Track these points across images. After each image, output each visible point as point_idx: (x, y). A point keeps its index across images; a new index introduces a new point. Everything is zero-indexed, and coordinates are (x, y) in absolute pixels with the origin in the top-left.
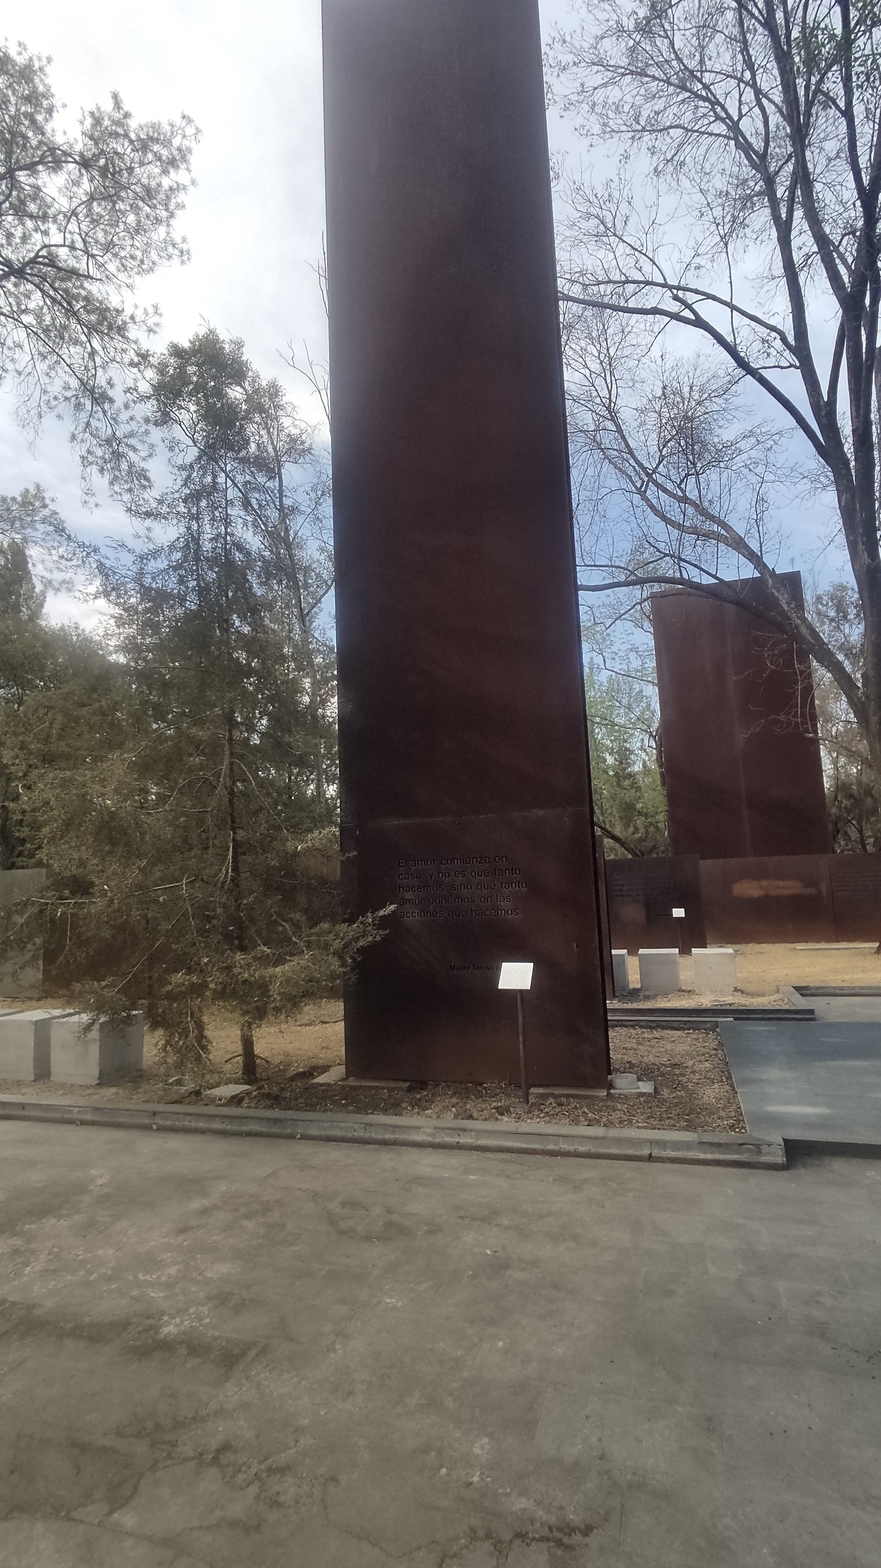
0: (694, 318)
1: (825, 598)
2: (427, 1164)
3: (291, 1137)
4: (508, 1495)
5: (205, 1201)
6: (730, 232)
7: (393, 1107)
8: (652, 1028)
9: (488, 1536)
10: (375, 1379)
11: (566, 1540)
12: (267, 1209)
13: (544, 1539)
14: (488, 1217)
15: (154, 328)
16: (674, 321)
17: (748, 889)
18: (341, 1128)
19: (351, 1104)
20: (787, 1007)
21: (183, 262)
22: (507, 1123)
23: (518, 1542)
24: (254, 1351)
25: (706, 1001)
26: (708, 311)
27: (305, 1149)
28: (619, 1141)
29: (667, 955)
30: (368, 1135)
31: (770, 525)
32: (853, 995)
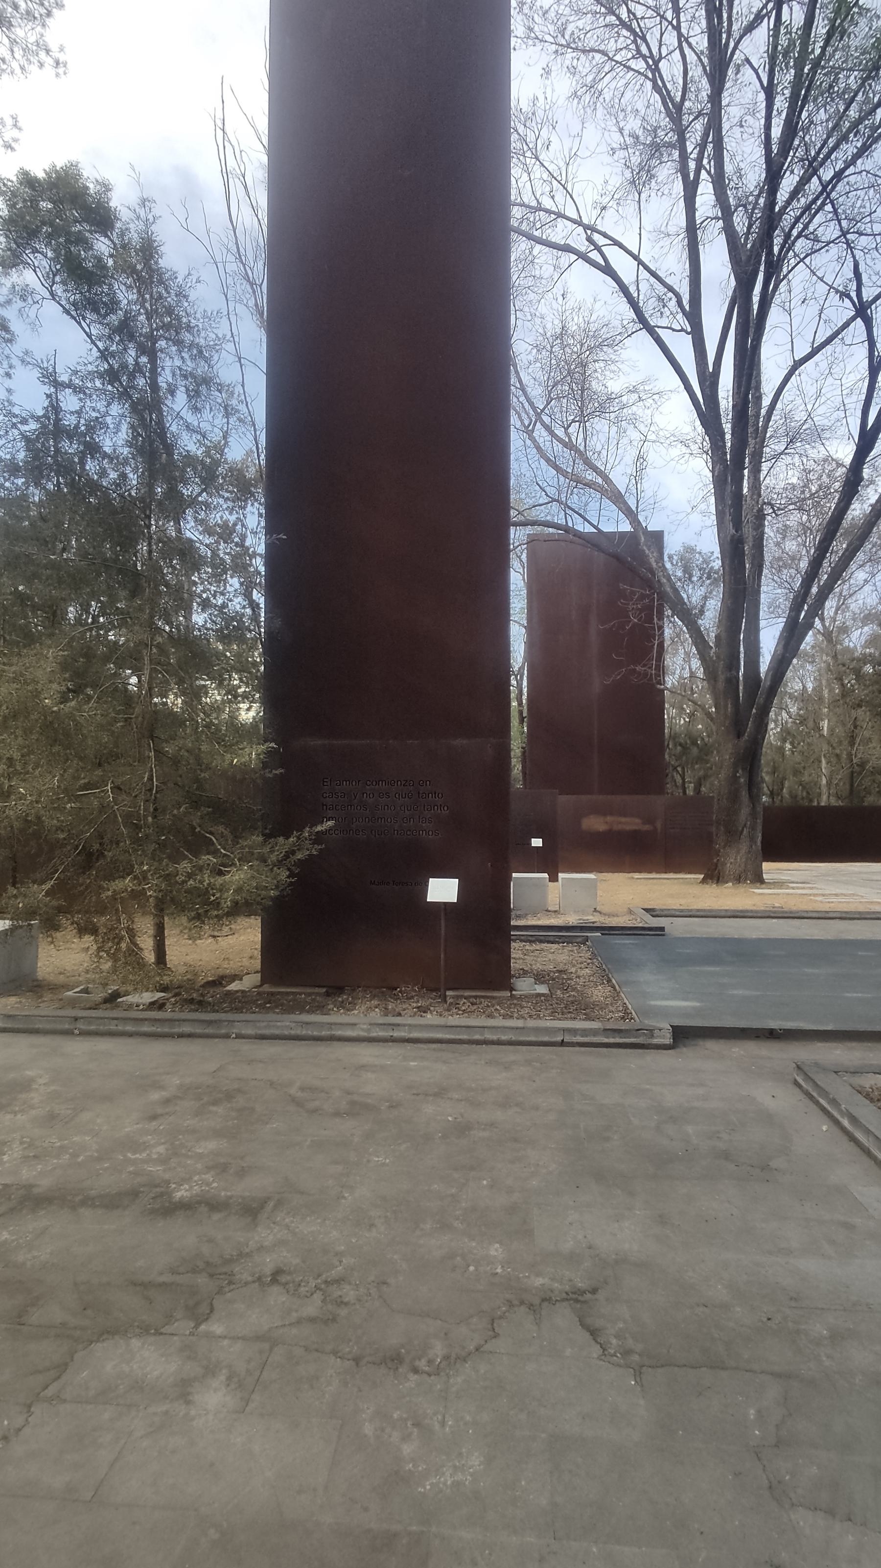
0: (603, 264)
1: (675, 558)
2: (367, 1054)
3: (227, 1036)
4: (528, 1277)
5: (164, 1093)
6: (640, 179)
7: (320, 1008)
8: (530, 942)
9: (522, 1303)
10: (388, 1214)
11: (580, 1298)
12: (229, 1096)
13: (563, 1300)
14: (440, 1093)
15: (13, 144)
16: (580, 260)
17: (595, 824)
18: (278, 1027)
19: (277, 1007)
20: (640, 925)
21: (57, 75)
22: (430, 1018)
23: (545, 1304)
24: (271, 1204)
25: (572, 919)
26: (615, 256)
27: (245, 1047)
28: (537, 1030)
29: (538, 878)
30: (304, 1032)
31: (647, 485)
32: (690, 916)
